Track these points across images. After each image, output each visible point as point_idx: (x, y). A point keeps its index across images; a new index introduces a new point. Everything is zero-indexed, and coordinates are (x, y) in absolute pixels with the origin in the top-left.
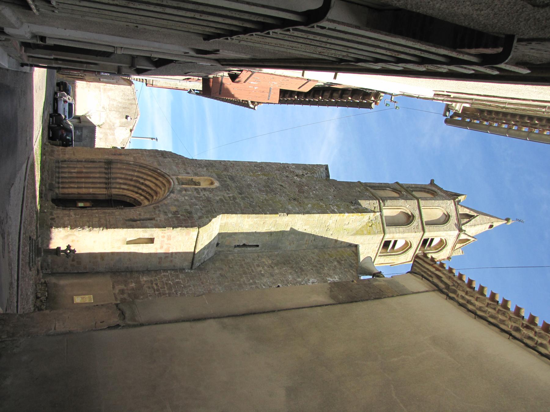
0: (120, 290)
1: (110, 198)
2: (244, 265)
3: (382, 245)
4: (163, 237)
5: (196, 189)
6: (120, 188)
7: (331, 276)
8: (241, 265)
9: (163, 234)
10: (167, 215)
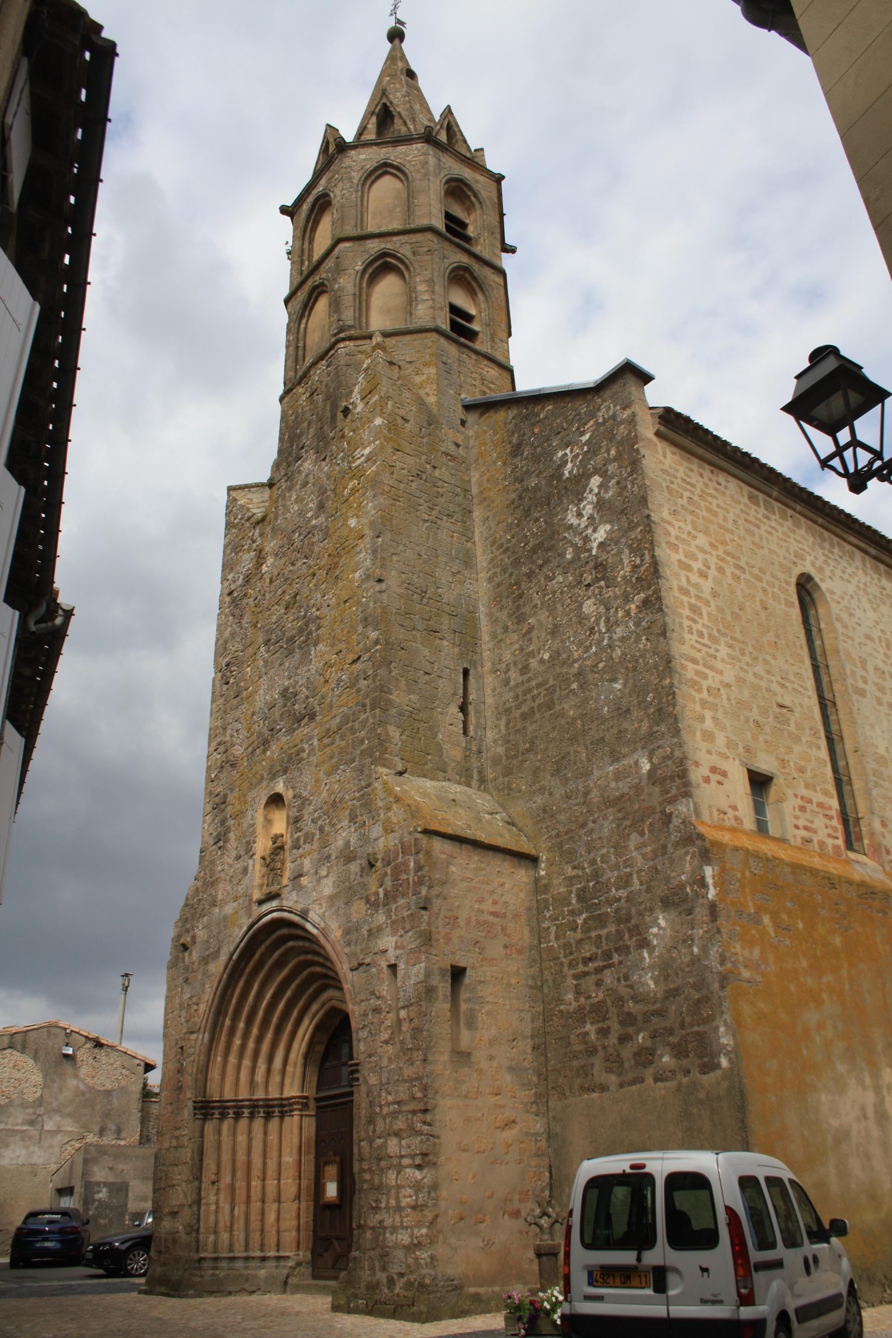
0: (609, 1071)
1: (312, 1104)
2: (525, 708)
3: (462, 340)
8: (524, 717)
10: (380, 929)
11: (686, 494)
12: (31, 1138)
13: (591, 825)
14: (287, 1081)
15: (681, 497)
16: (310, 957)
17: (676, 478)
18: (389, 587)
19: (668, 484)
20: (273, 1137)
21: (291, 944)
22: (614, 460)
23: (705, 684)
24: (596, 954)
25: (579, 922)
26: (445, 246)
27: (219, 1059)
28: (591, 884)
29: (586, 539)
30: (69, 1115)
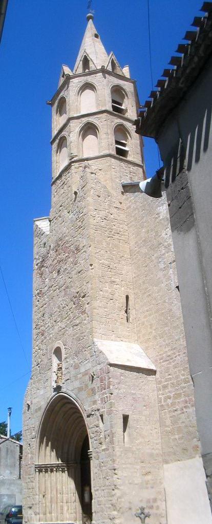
3: (121, 157)
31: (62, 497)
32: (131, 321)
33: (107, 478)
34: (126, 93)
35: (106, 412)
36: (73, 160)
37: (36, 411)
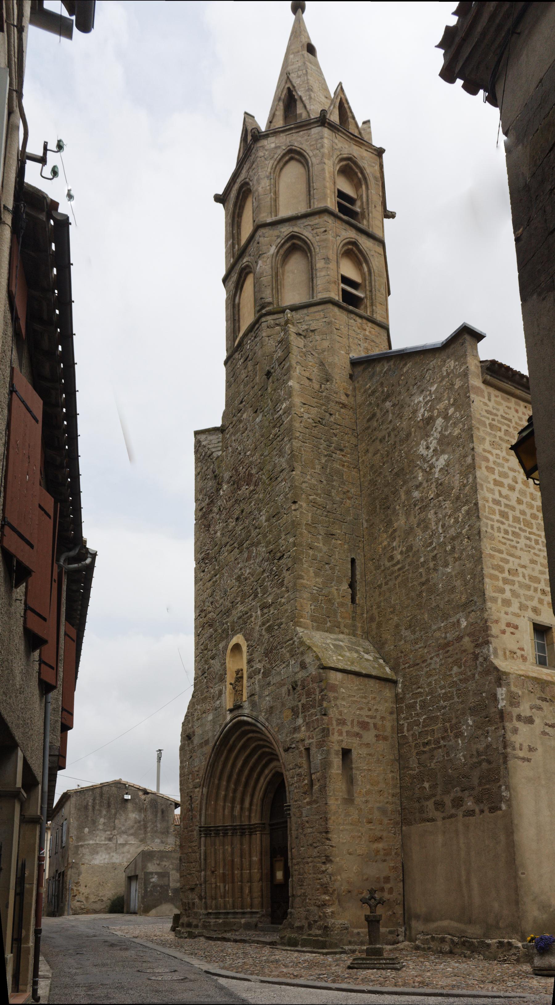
3: (351, 308)
4: (341, 734)
5: (250, 677)
6: (250, 810)
7: (415, 412)
9: (336, 734)
11: (504, 428)
12: (110, 848)
13: (429, 661)
14: (253, 815)
15: (500, 430)
16: (261, 743)
17: (497, 416)
18: (301, 506)
19: (490, 421)
20: (246, 847)
21: (250, 735)
22: (453, 405)
23: (507, 567)
24: (430, 740)
25: (421, 721)
26: (337, 225)
27: (214, 791)
28: (428, 698)
29: (432, 467)
30: (132, 834)
31: (242, 874)
32: (357, 602)
33: (315, 845)
34: (365, 179)
35: (314, 743)
36: (264, 311)
37: (201, 746)
